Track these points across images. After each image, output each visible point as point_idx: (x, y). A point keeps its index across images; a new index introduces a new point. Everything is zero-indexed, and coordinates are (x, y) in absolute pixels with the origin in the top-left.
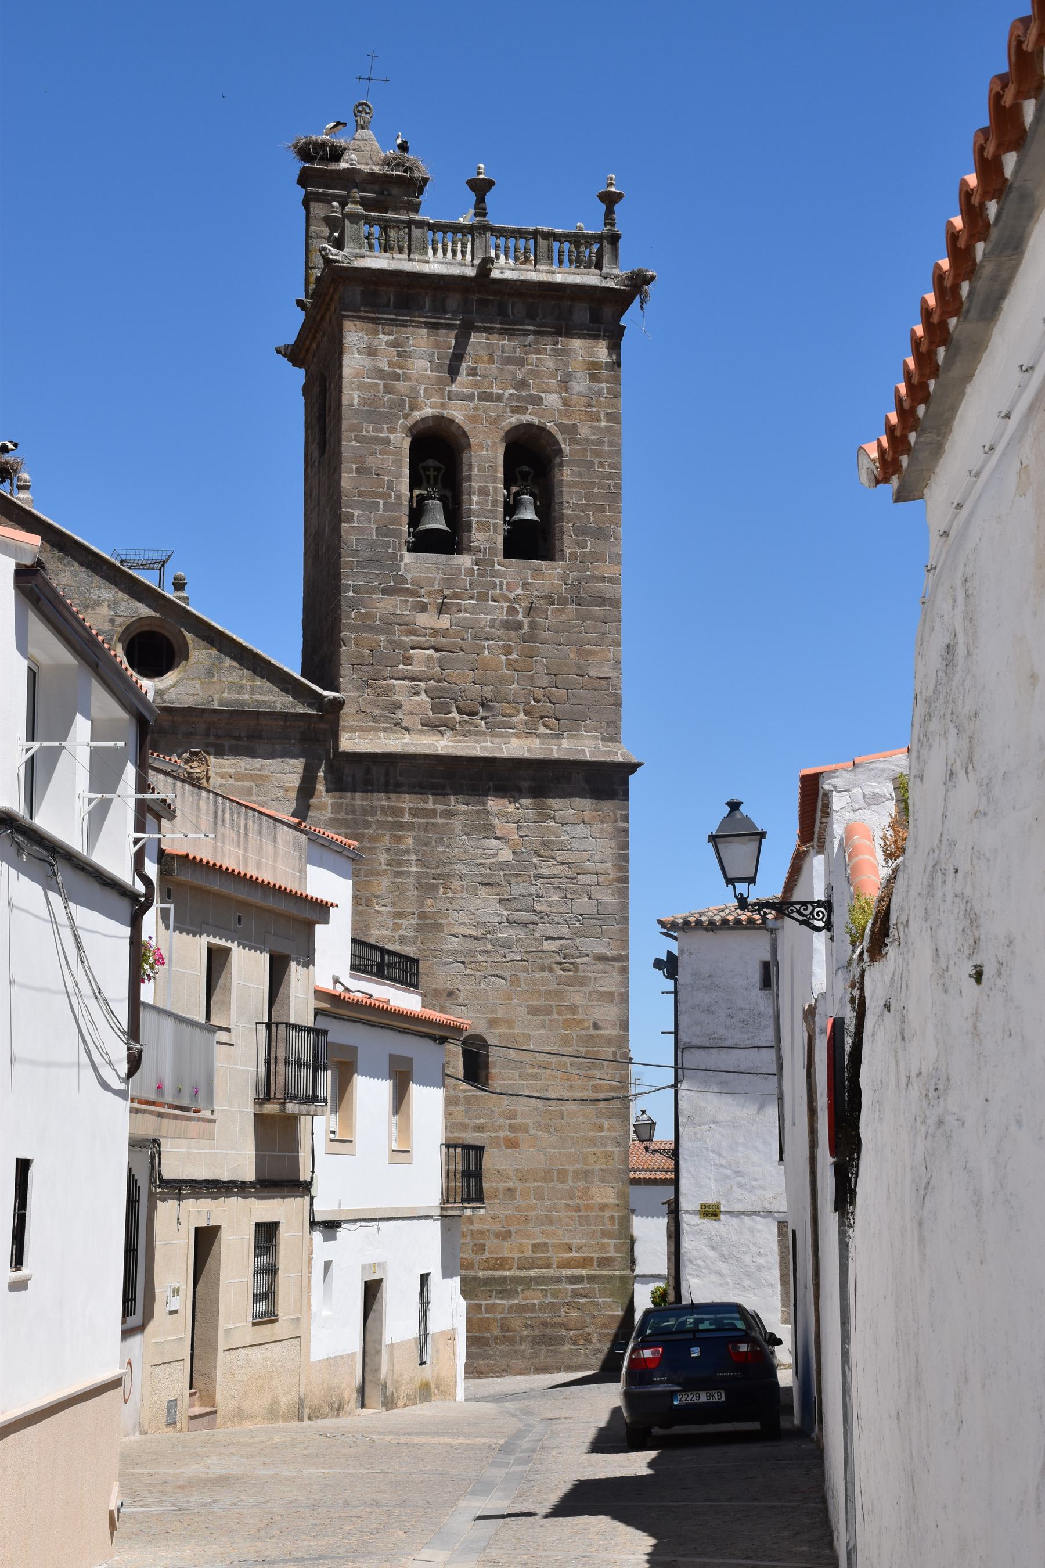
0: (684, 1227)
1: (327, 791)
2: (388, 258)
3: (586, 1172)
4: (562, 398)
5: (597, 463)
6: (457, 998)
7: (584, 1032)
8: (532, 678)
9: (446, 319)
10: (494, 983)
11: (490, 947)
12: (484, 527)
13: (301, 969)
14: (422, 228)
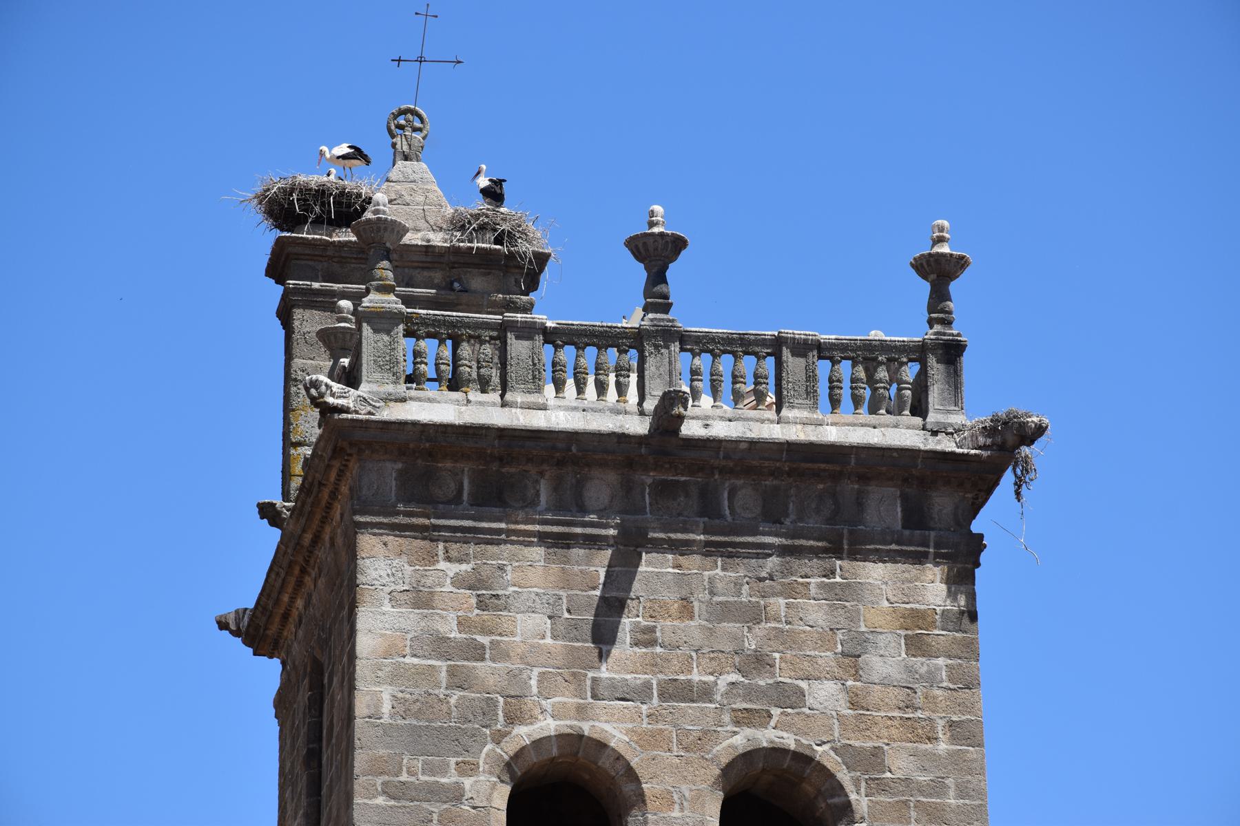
2: (457, 402)
4: (847, 690)
9: (585, 525)
14: (530, 338)
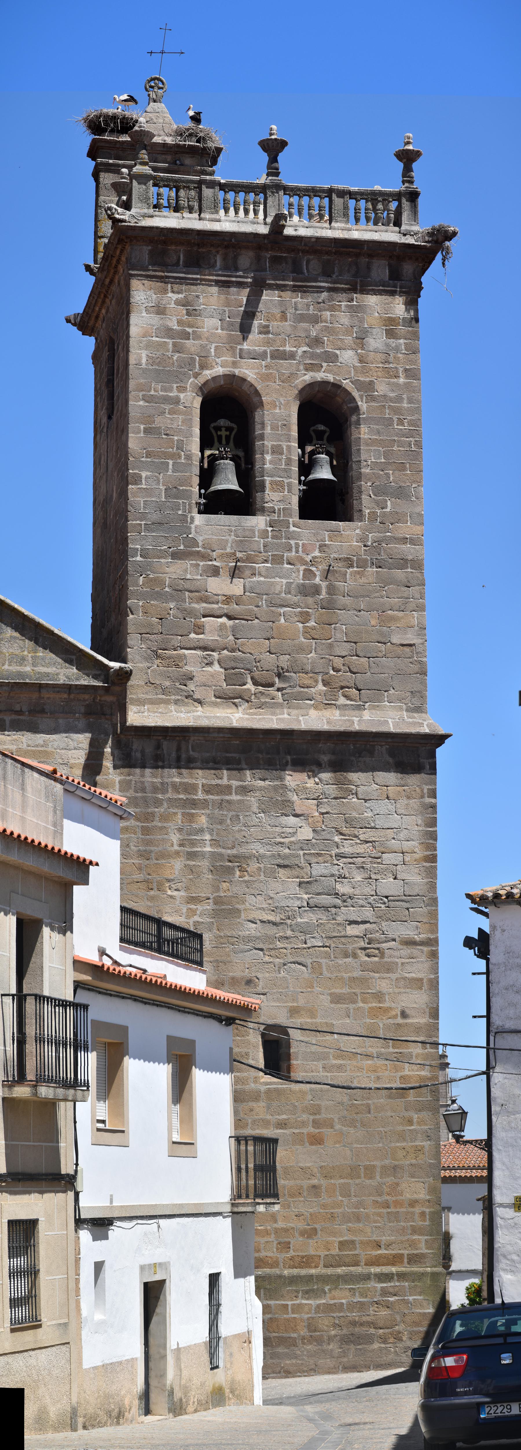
0: (498, 1221)
1: (115, 767)
3: (395, 1168)
5: (396, 420)
6: (256, 986)
7: (391, 1021)
8: (331, 646)
10: (294, 971)
11: (289, 933)
12: (279, 486)
13: (56, 936)
14: (213, 188)
